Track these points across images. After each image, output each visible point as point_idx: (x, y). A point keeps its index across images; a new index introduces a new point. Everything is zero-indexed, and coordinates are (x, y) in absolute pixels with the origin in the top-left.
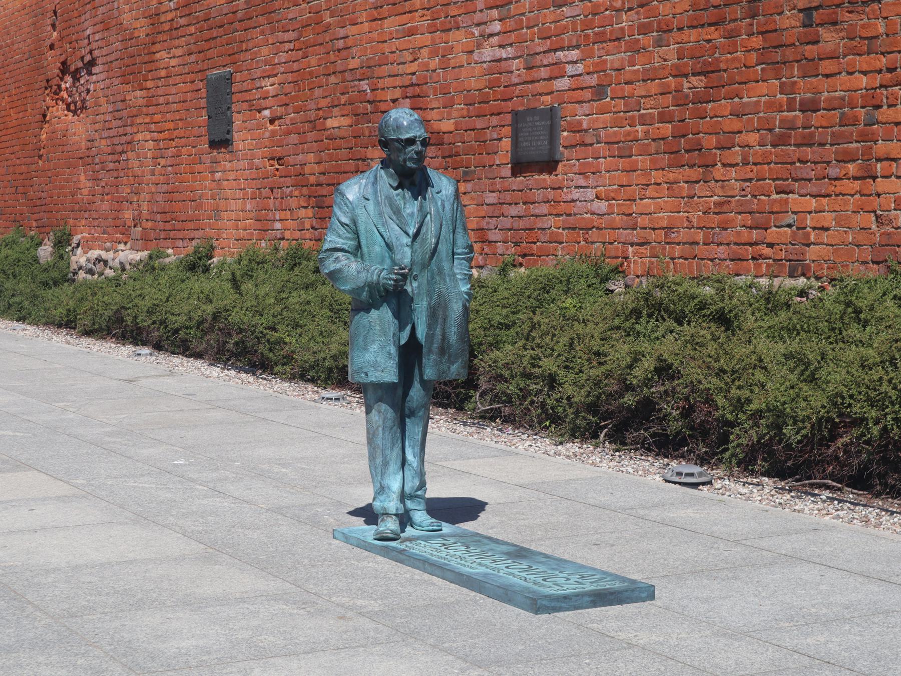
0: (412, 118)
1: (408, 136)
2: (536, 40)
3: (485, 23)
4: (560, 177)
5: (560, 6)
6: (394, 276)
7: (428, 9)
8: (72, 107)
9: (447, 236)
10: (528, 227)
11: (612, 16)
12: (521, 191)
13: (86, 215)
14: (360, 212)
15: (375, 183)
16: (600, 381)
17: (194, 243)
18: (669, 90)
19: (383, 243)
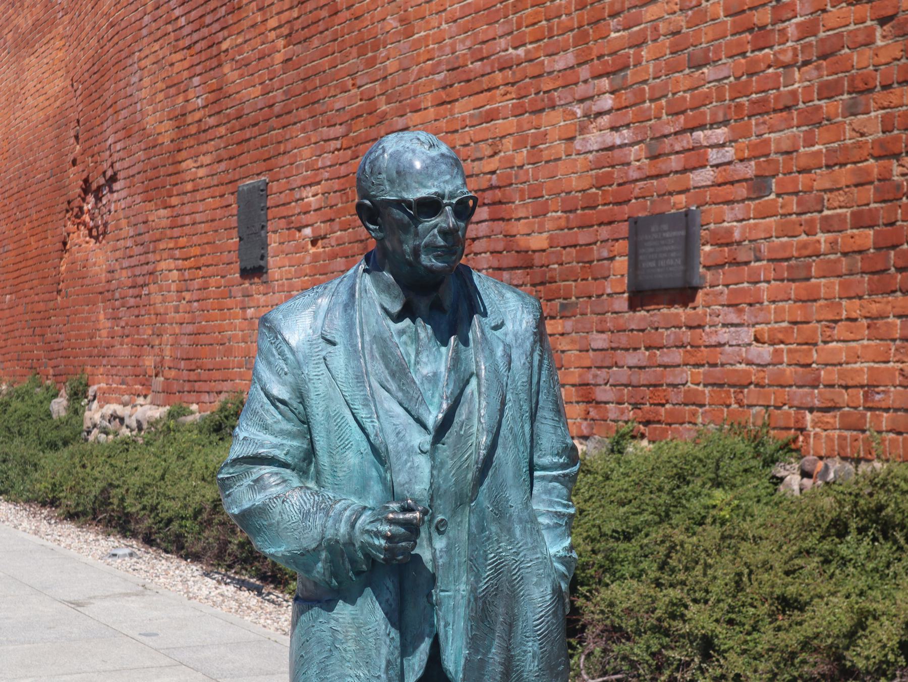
0: (434, 153)
1: (423, 193)
2: (664, 117)
3: (591, 98)
4: (700, 310)
5: (699, 67)
6: (386, 528)
7: (513, 84)
8: (94, 233)
9: (517, 429)
10: (653, 382)
11: (778, 75)
12: (643, 330)
13: (104, 362)
14: (313, 371)
15: (349, 304)
16: (793, 655)
17: (223, 397)
18: (869, 179)
19: (365, 446)
